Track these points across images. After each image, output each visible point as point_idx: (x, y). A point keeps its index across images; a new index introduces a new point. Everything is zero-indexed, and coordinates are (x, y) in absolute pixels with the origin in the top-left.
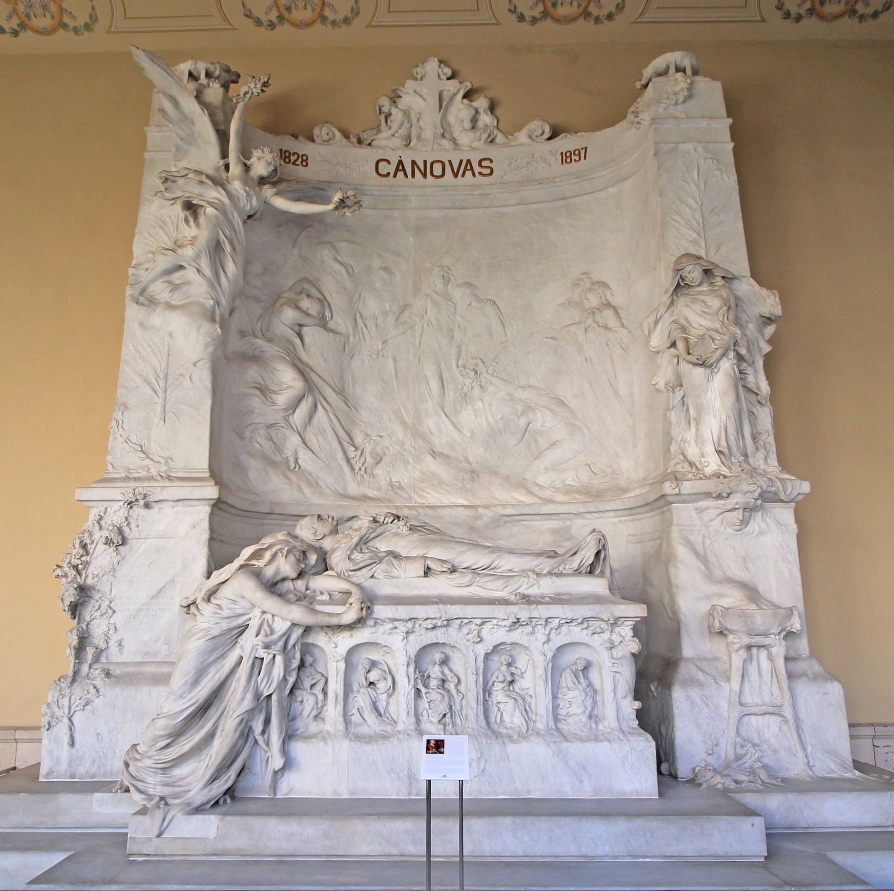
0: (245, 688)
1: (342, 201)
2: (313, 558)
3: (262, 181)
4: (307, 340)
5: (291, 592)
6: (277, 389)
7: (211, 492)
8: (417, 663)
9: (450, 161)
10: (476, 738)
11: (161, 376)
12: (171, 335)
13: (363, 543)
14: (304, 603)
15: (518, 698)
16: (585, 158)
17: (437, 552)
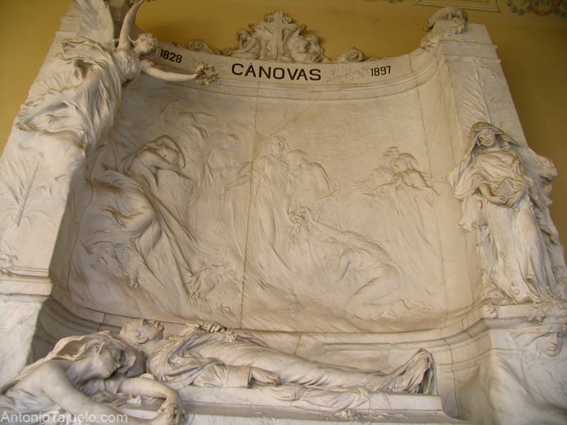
2: (131, 360)
3: (142, 56)
4: (161, 180)
5: (101, 392)
6: (128, 215)
7: (45, 288)
9: (288, 70)
11: (26, 186)
12: (42, 155)
13: (186, 348)
14: (113, 405)
17: (263, 363)
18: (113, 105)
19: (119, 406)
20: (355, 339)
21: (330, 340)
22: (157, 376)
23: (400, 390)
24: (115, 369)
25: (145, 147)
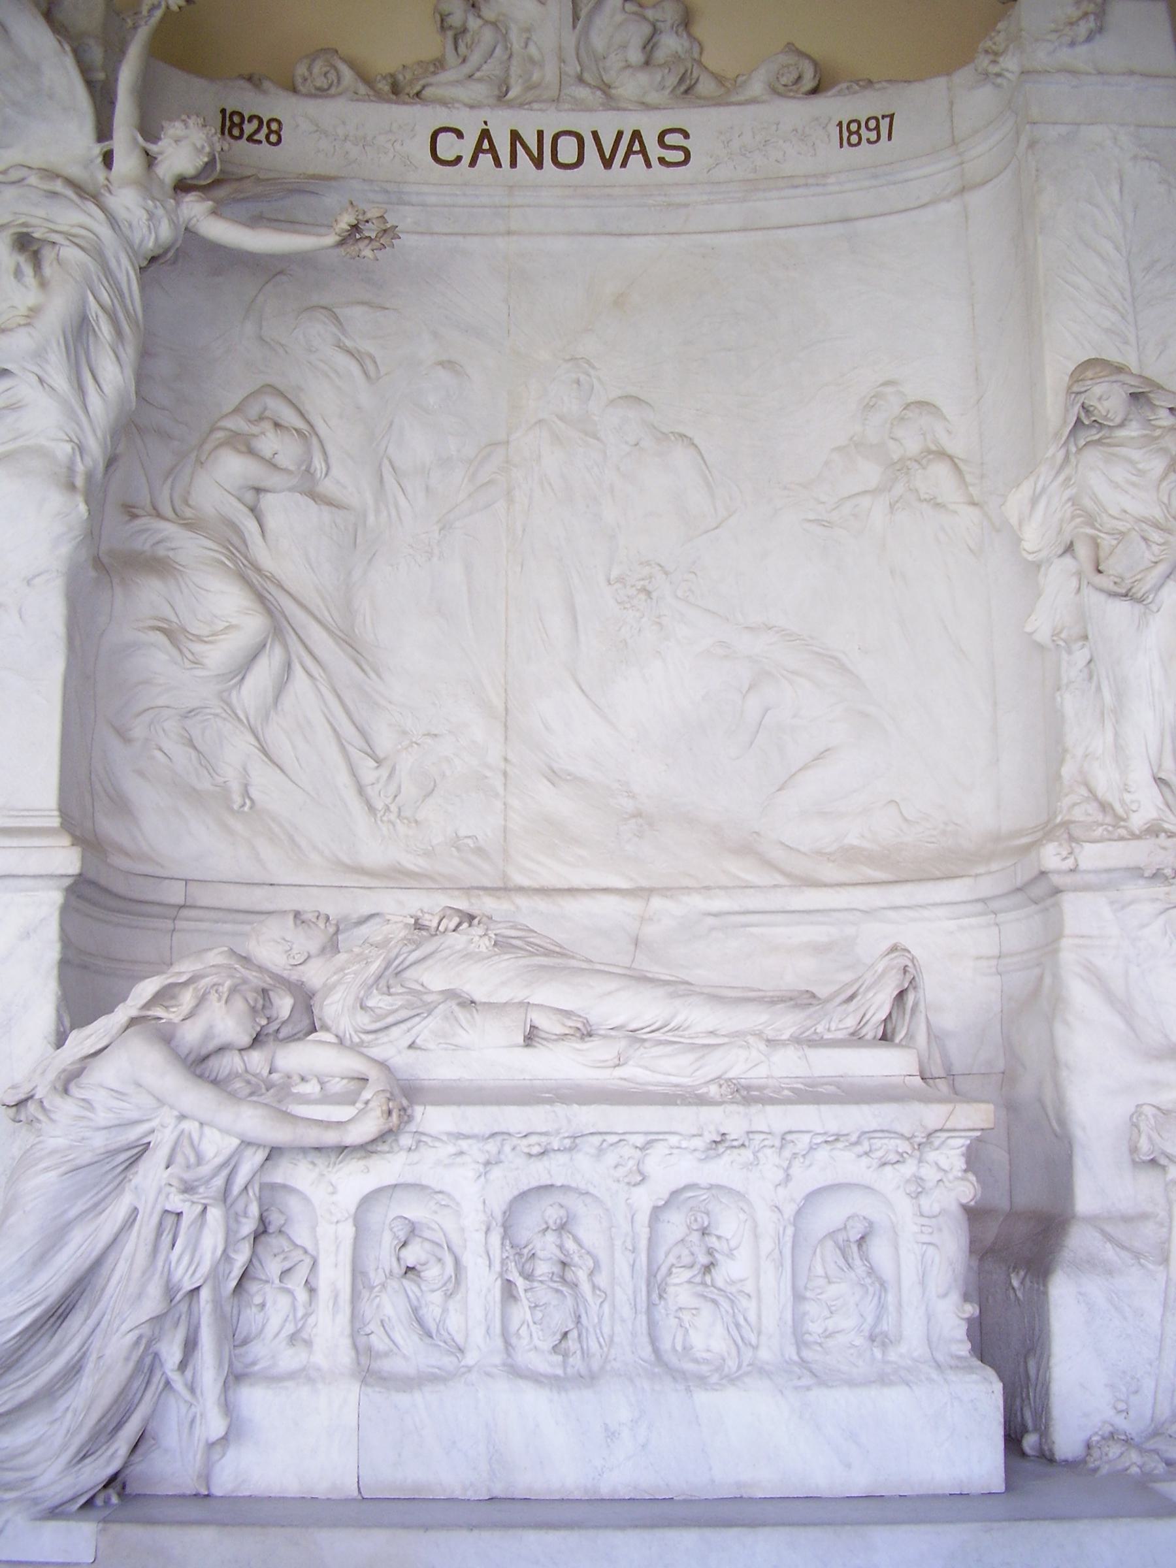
0: (144, 1273)
1: (355, 228)
2: (284, 1005)
3: (183, 186)
4: (271, 523)
5: (238, 1075)
6: (203, 631)
7: (66, 860)
8: (506, 1227)
9: (595, 134)
10: (631, 1380)
13: (391, 975)
14: (268, 1097)
15: (721, 1300)
16: (890, 138)
17: (553, 994)
18: (129, 353)
19: (279, 1101)
20: (777, 900)
21: (720, 903)
22: (341, 1034)
23: (840, 1035)
24: (258, 1029)
25: (220, 435)
